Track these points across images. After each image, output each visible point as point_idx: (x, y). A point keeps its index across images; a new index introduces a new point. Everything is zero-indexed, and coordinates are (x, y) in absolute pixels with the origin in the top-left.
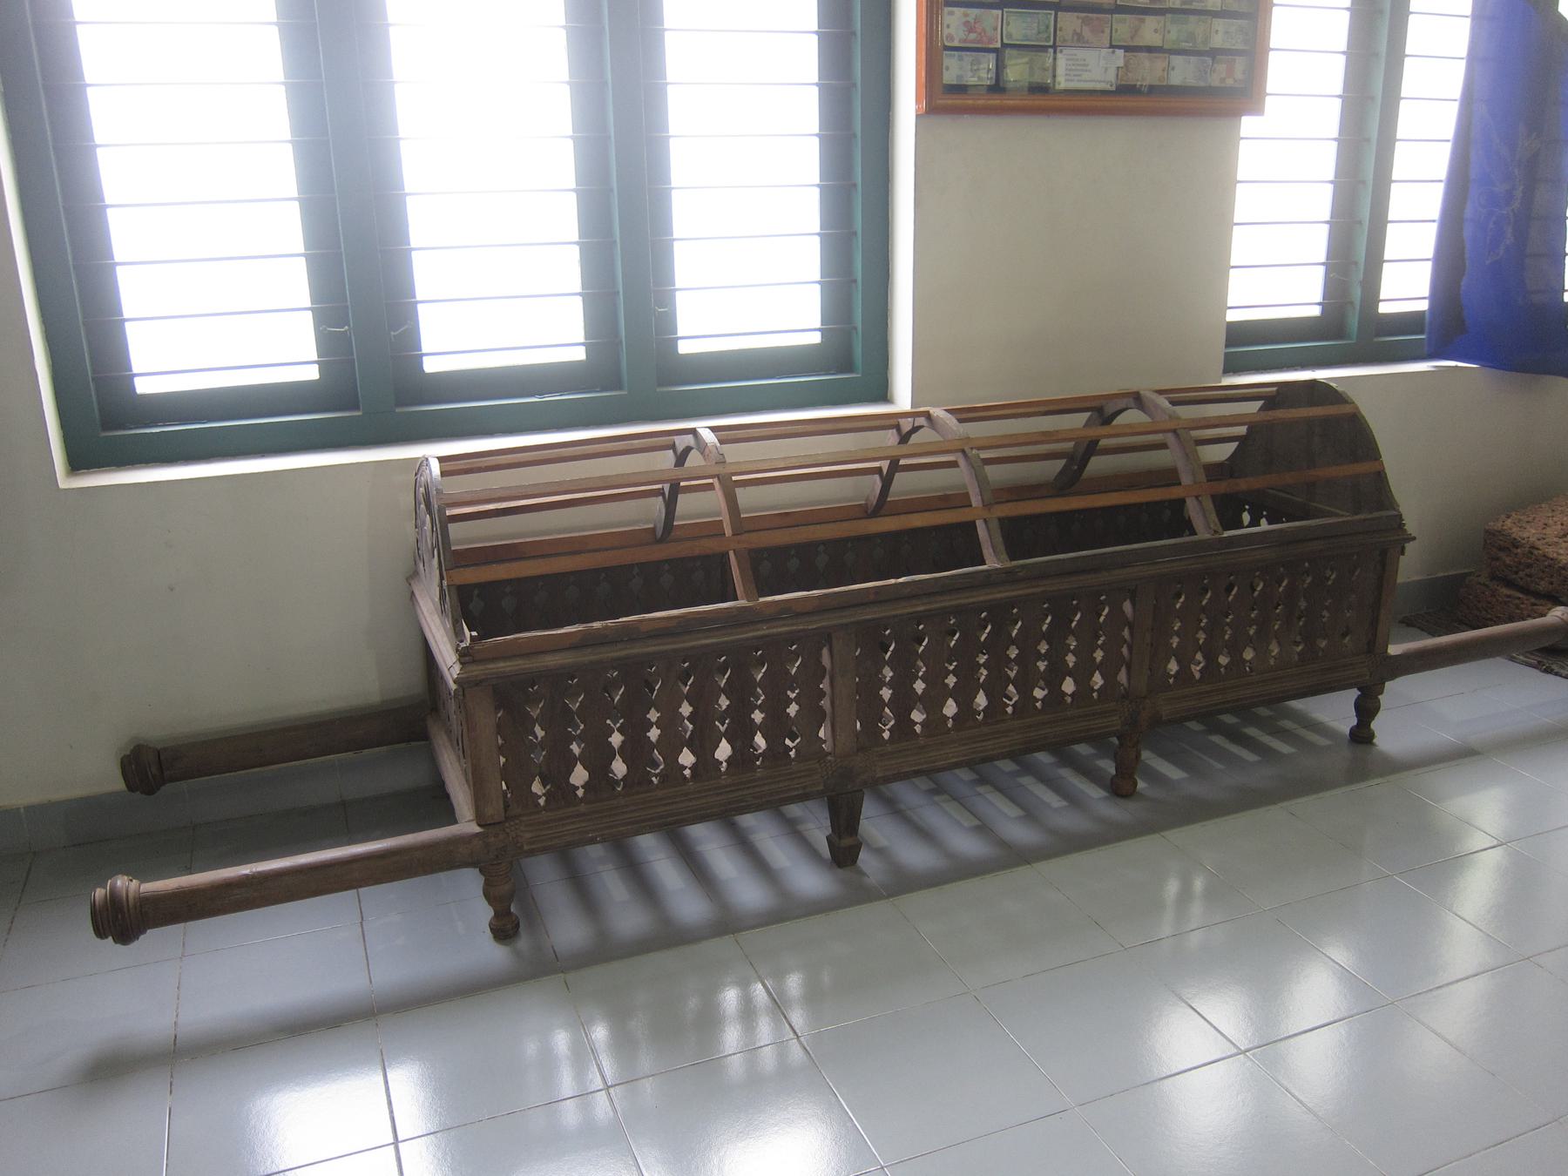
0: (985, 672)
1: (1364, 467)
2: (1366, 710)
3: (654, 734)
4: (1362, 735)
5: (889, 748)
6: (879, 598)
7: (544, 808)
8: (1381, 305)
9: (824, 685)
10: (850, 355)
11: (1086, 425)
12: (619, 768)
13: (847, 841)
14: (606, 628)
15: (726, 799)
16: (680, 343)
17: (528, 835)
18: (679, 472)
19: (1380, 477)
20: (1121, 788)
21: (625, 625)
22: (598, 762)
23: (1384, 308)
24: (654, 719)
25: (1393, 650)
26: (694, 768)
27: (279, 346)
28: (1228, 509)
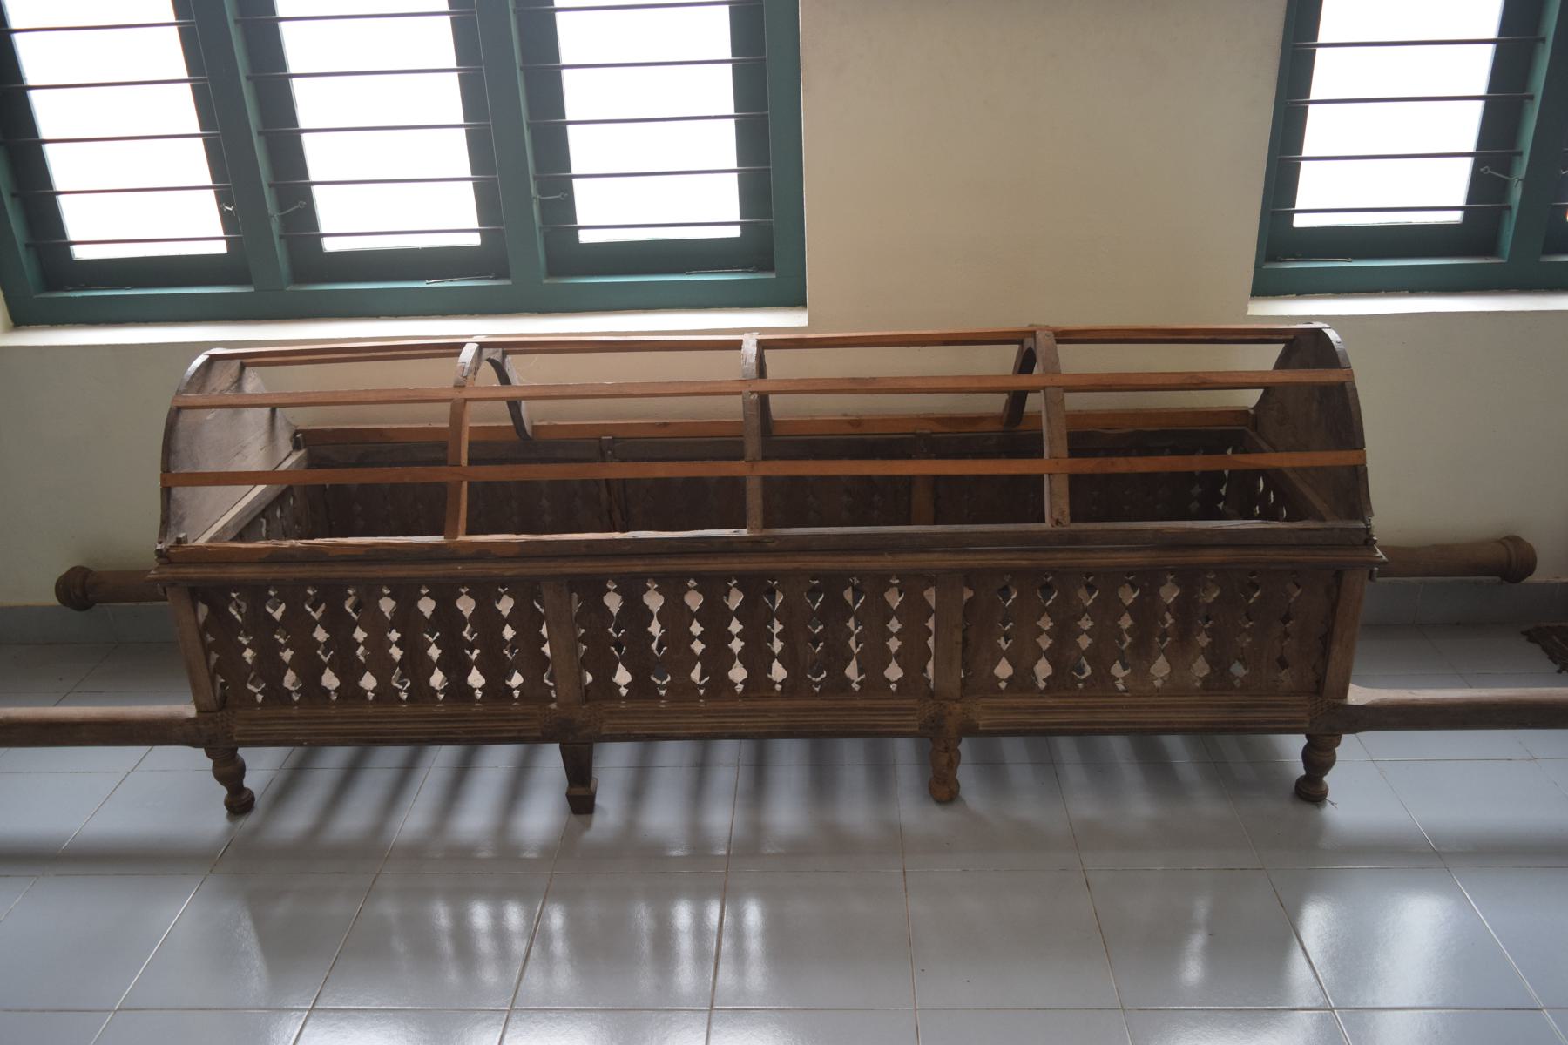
0: (1129, 640)
1: (1343, 458)
2: (1319, 759)
3: (1084, 642)
4: (1311, 791)
5: (623, 706)
6: (592, 551)
7: (261, 705)
8: (1297, 217)
9: (931, 624)
10: (764, 257)
11: (1277, 367)
12: (778, 672)
13: (580, 791)
14: (292, 548)
15: (468, 727)
16: (581, 232)
17: (239, 728)
18: (1024, 381)
19: (1358, 474)
20: (942, 790)
21: (313, 548)
22: (874, 662)
23: (1299, 221)
24: (895, 630)
25: (1358, 695)
26: (1010, 680)
27: (449, 215)
28: (1092, 498)
